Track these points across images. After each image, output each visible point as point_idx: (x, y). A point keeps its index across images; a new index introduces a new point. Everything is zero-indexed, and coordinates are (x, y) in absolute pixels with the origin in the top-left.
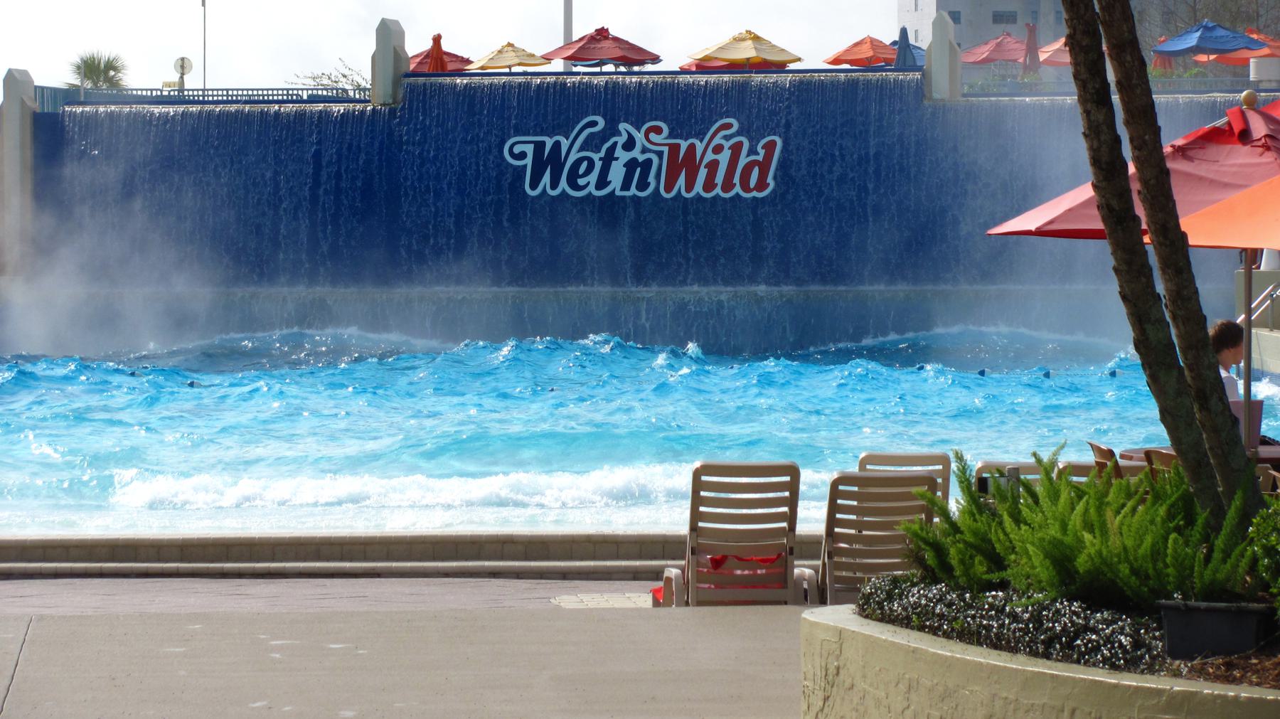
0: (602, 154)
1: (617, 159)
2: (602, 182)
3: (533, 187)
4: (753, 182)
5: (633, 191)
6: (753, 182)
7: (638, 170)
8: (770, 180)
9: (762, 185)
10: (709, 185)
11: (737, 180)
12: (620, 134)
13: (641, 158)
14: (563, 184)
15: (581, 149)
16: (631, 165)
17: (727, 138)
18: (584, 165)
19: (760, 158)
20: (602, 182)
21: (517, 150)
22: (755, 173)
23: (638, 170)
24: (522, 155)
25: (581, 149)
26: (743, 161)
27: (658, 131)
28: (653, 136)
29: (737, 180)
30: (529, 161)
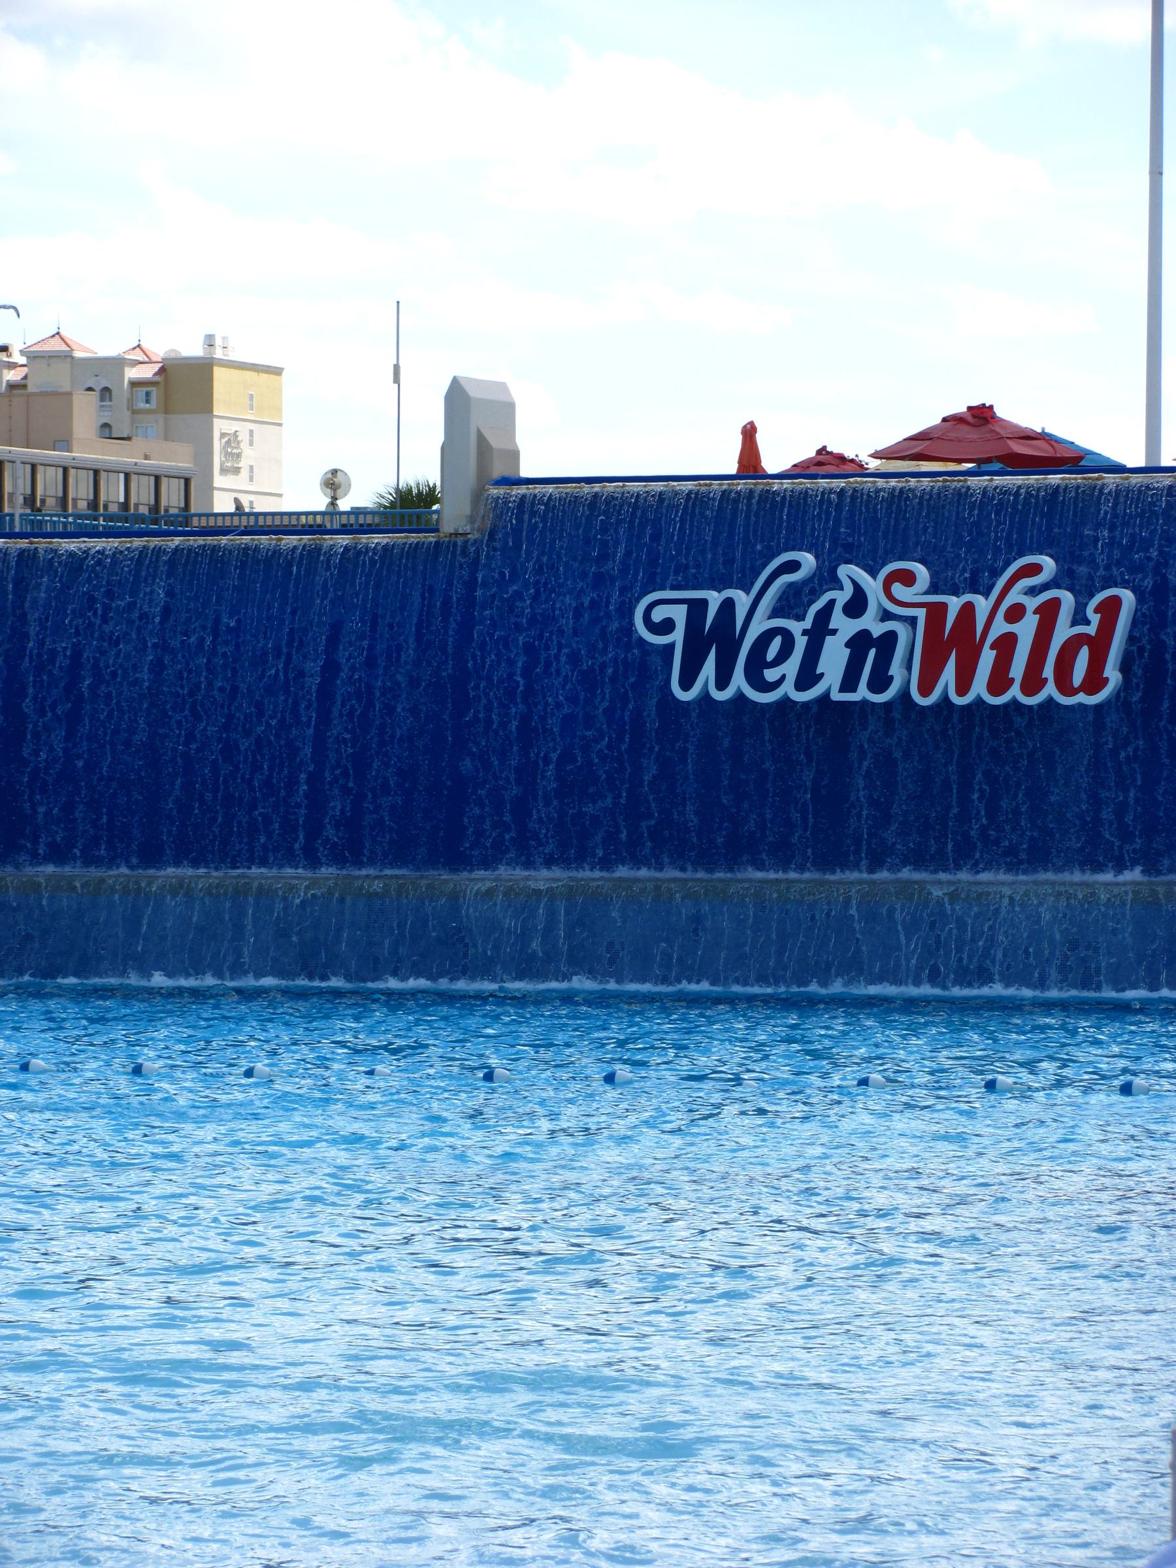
0: (808, 623)
2: (808, 676)
3: (686, 684)
5: (862, 692)
7: (872, 653)
11: (1048, 671)
18: (777, 643)
19: (1091, 630)
20: (808, 676)
21: (658, 615)
24: (667, 626)
29: (1048, 671)
30: (677, 636)
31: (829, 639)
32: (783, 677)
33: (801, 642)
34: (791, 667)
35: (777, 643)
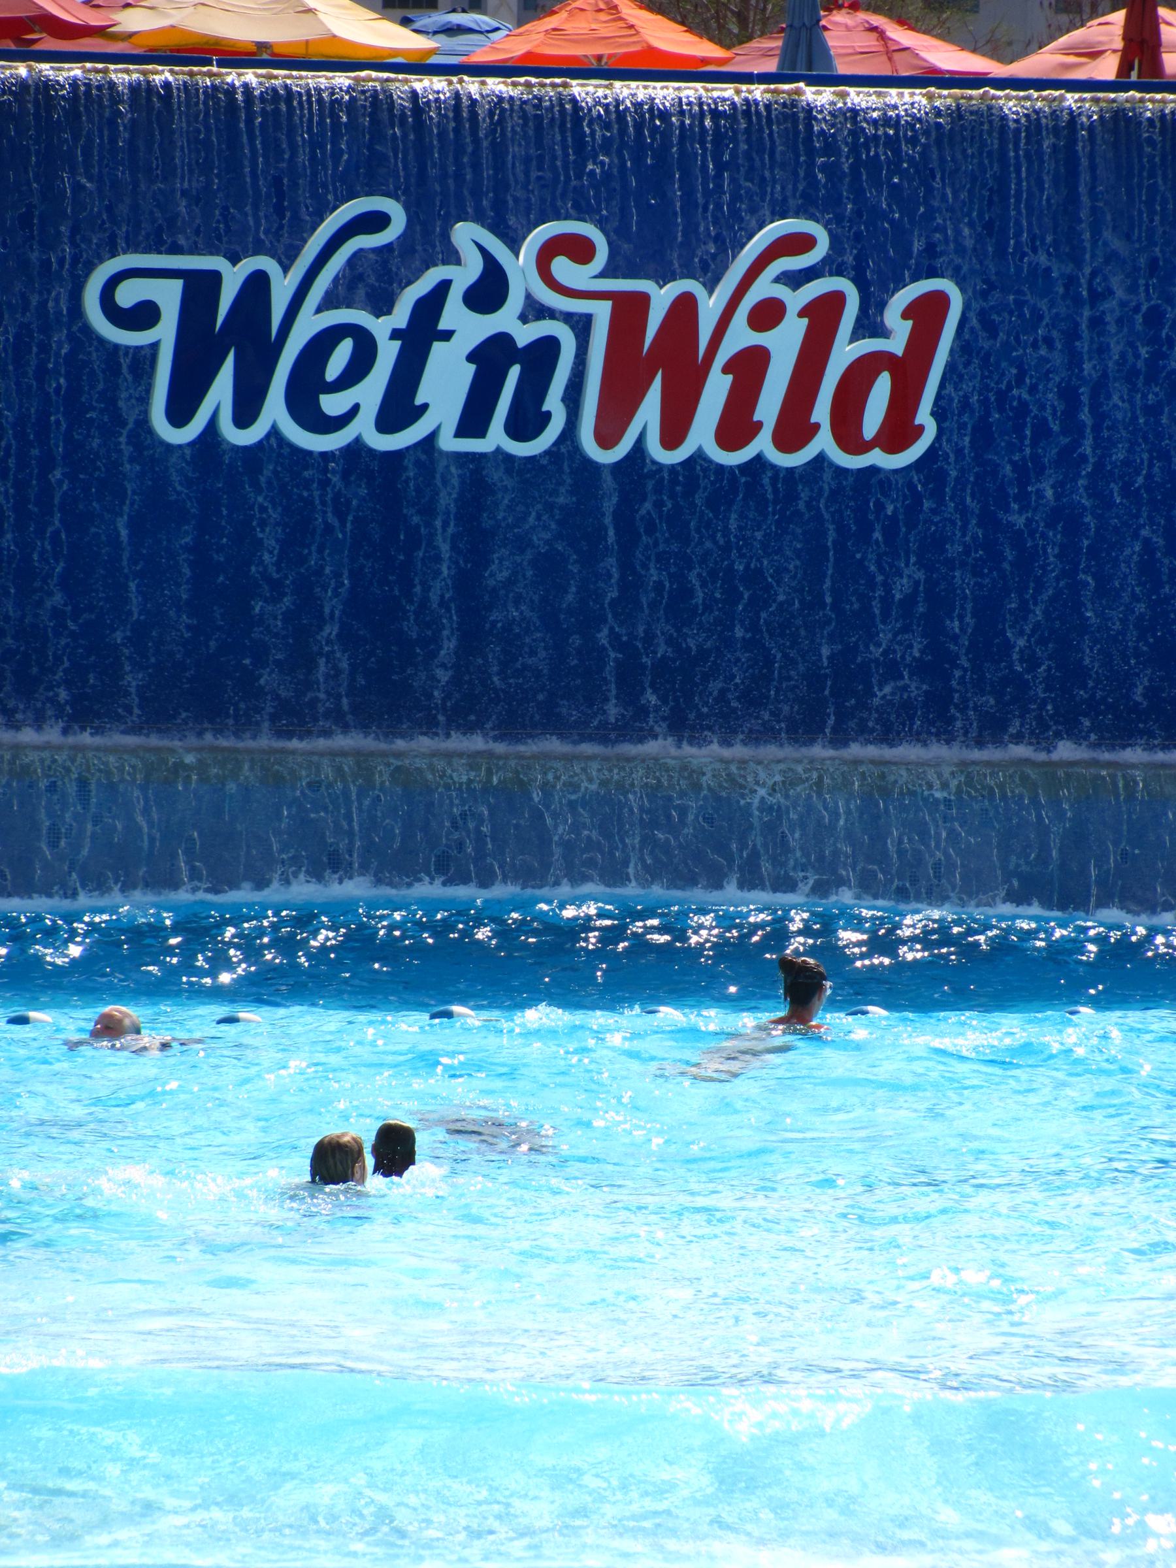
0: (400, 316)
1: (447, 335)
2: (399, 408)
5: (496, 438)
8: (924, 416)
9: (898, 432)
10: (736, 426)
11: (821, 412)
12: (452, 257)
14: (275, 409)
15: (329, 302)
16: (491, 357)
17: (795, 280)
20: (399, 408)
21: (128, 295)
22: (883, 386)
23: (515, 372)
24: (145, 315)
25: (329, 302)
26: (845, 351)
27: (580, 250)
28: (562, 267)
29: (821, 412)
30: (165, 333)
31: (437, 347)
32: (355, 409)
33: (388, 353)
34: (370, 392)
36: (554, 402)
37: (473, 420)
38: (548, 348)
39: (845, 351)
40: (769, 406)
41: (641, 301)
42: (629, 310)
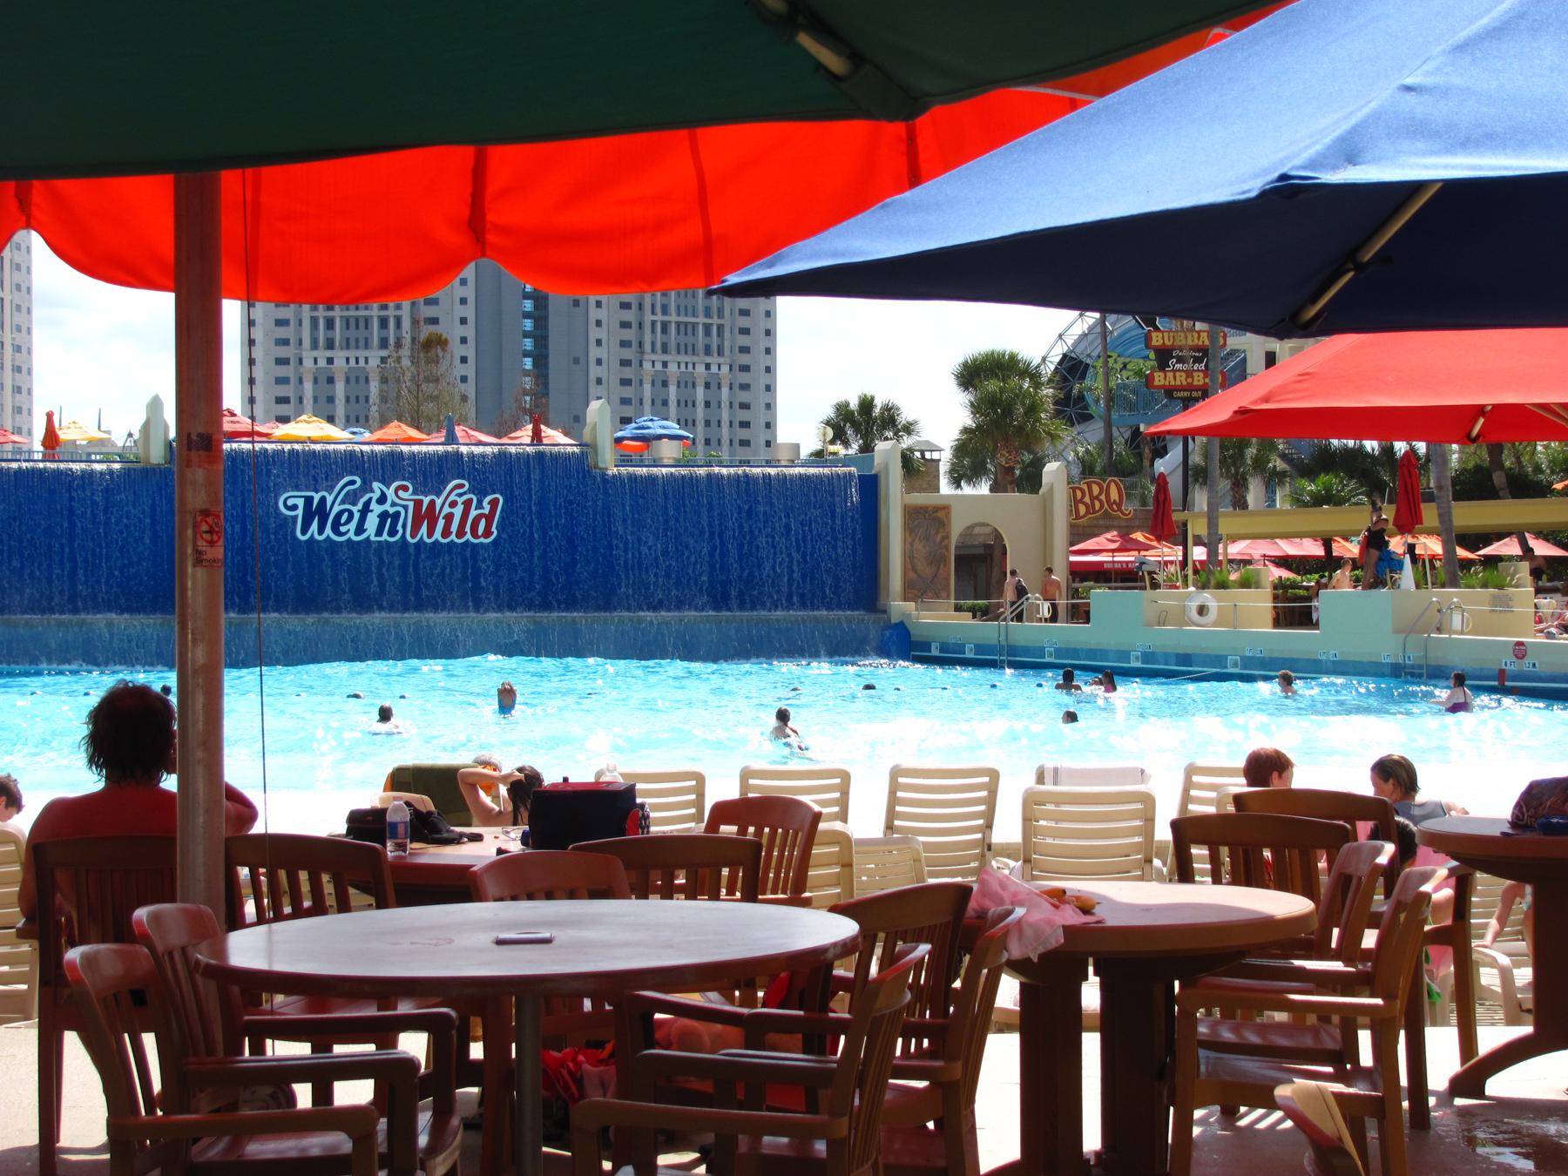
0: (360, 506)
4: (481, 531)
5: (385, 537)
6: (481, 531)
9: (487, 533)
11: (468, 529)
12: (372, 491)
13: (392, 510)
14: (328, 530)
15: (343, 502)
16: (383, 516)
17: (460, 495)
20: (360, 530)
21: (290, 502)
22: (483, 523)
24: (295, 507)
25: (343, 502)
26: (473, 513)
27: (405, 489)
28: (401, 493)
29: (468, 529)
30: (300, 512)
33: (357, 516)
34: (353, 526)
35: (345, 517)
36: (399, 528)
37: (379, 532)
38: (397, 514)
39: (473, 513)
40: (454, 527)
41: (421, 502)
42: (418, 504)
